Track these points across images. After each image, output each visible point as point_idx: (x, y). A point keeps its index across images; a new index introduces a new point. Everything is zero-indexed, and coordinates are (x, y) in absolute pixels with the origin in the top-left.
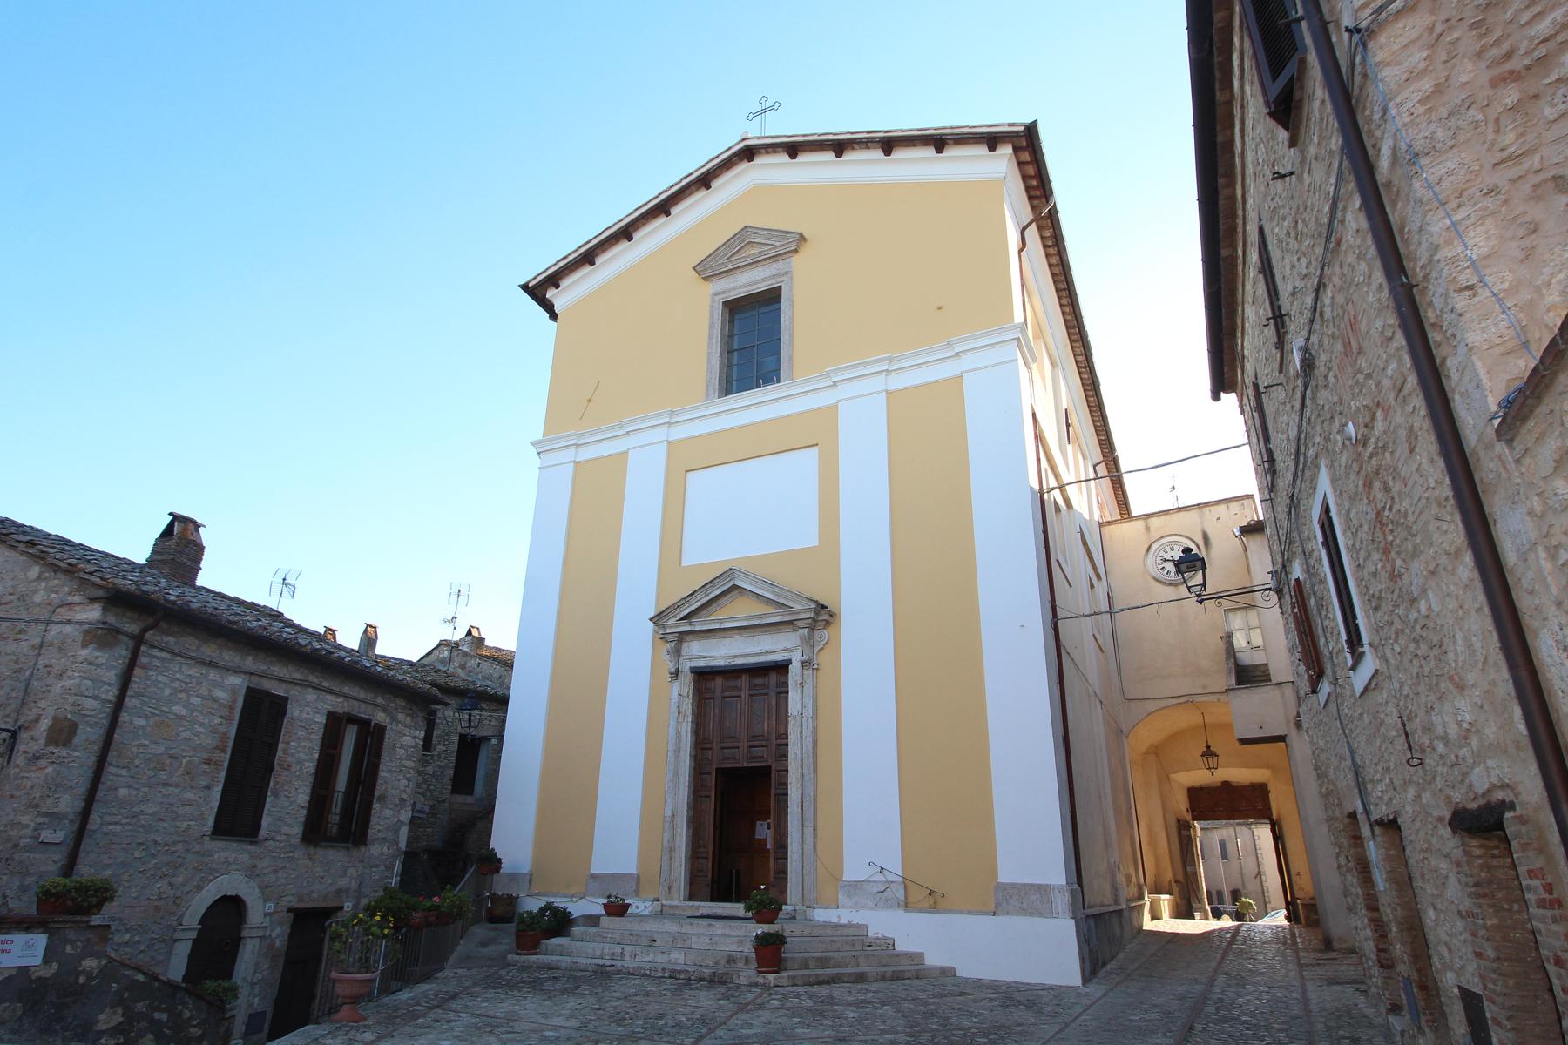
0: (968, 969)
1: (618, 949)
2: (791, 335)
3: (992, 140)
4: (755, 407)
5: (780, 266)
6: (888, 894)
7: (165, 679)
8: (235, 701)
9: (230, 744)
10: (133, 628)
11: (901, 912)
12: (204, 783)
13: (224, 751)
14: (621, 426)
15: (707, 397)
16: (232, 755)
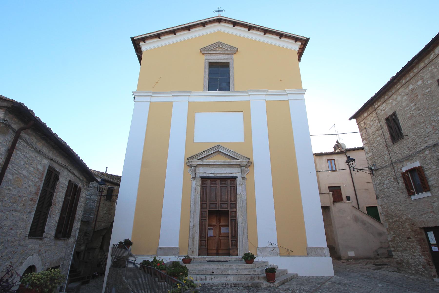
1: (203, 277)
2: (233, 77)
3: (296, 39)
4: (219, 96)
5: (229, 56)
6: (274, 251)
7: (22, 156)
8: (44, 172)
9: (40, 192)
10: (15, 127)
11: (279, 257)
12: (29, 210)
13: (37, 195)
14: (171, 93)
15: (204, 90)
16: (40, 197)
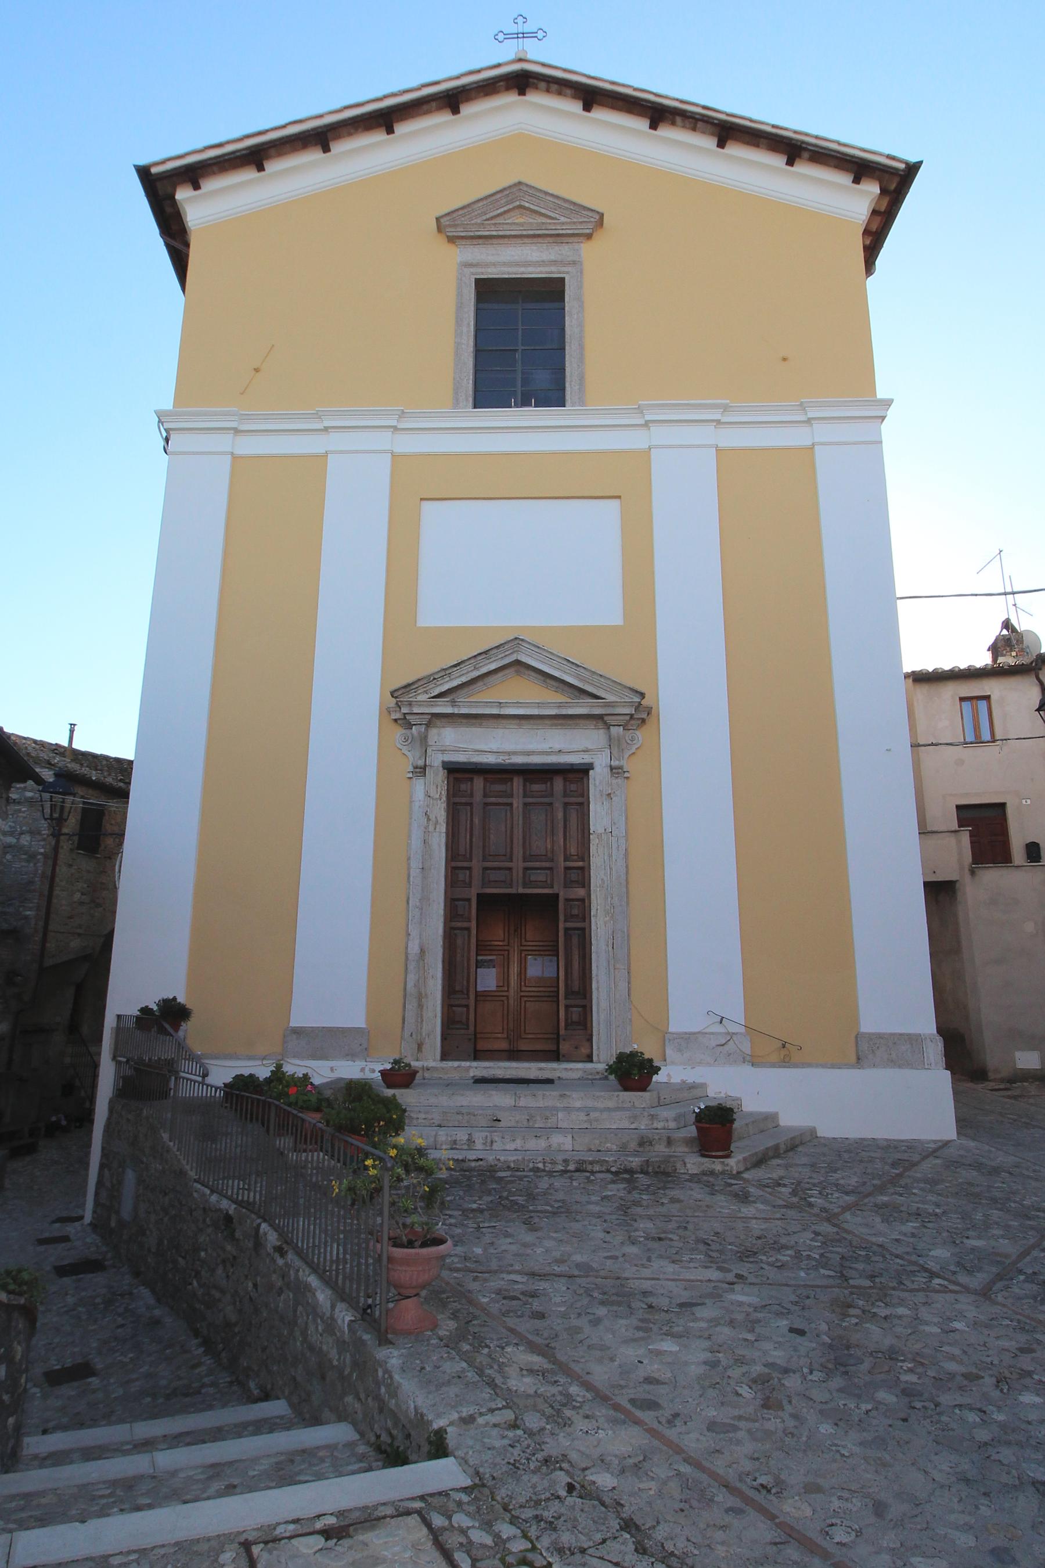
0: (830, 1128)
1: (462, 1136)
2: (582, 347)
4: (520, 431)
5: (564, 251)
11: (748, 1069)
14: (318, 416)
15: (456, 404)
